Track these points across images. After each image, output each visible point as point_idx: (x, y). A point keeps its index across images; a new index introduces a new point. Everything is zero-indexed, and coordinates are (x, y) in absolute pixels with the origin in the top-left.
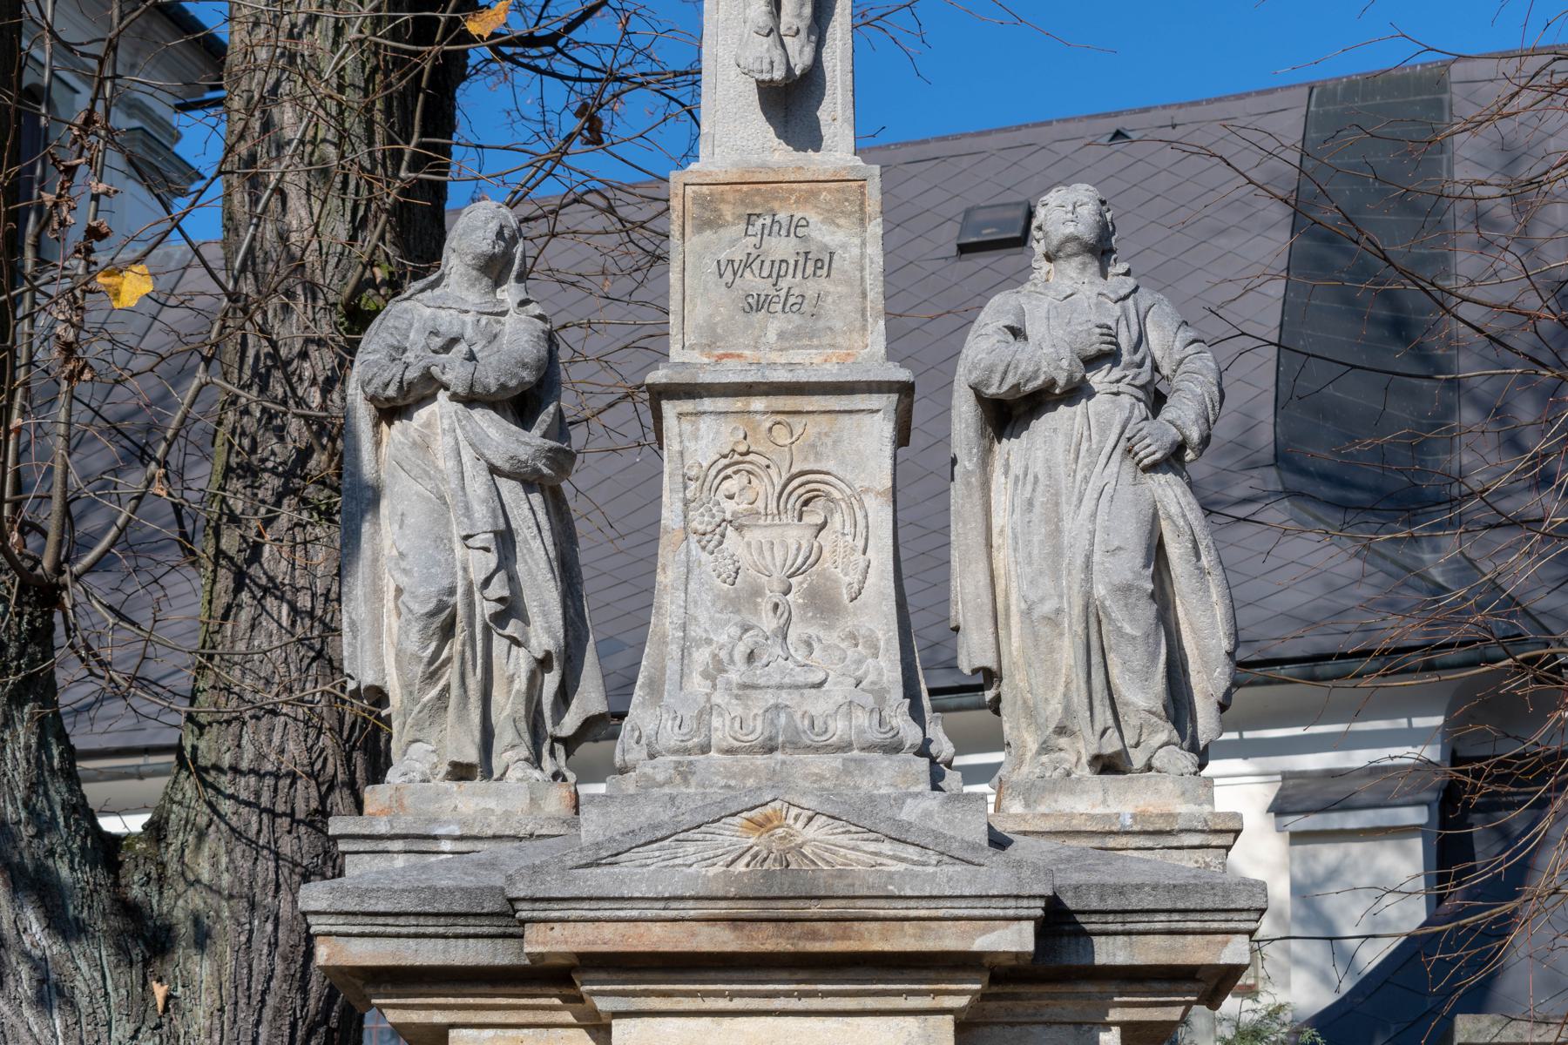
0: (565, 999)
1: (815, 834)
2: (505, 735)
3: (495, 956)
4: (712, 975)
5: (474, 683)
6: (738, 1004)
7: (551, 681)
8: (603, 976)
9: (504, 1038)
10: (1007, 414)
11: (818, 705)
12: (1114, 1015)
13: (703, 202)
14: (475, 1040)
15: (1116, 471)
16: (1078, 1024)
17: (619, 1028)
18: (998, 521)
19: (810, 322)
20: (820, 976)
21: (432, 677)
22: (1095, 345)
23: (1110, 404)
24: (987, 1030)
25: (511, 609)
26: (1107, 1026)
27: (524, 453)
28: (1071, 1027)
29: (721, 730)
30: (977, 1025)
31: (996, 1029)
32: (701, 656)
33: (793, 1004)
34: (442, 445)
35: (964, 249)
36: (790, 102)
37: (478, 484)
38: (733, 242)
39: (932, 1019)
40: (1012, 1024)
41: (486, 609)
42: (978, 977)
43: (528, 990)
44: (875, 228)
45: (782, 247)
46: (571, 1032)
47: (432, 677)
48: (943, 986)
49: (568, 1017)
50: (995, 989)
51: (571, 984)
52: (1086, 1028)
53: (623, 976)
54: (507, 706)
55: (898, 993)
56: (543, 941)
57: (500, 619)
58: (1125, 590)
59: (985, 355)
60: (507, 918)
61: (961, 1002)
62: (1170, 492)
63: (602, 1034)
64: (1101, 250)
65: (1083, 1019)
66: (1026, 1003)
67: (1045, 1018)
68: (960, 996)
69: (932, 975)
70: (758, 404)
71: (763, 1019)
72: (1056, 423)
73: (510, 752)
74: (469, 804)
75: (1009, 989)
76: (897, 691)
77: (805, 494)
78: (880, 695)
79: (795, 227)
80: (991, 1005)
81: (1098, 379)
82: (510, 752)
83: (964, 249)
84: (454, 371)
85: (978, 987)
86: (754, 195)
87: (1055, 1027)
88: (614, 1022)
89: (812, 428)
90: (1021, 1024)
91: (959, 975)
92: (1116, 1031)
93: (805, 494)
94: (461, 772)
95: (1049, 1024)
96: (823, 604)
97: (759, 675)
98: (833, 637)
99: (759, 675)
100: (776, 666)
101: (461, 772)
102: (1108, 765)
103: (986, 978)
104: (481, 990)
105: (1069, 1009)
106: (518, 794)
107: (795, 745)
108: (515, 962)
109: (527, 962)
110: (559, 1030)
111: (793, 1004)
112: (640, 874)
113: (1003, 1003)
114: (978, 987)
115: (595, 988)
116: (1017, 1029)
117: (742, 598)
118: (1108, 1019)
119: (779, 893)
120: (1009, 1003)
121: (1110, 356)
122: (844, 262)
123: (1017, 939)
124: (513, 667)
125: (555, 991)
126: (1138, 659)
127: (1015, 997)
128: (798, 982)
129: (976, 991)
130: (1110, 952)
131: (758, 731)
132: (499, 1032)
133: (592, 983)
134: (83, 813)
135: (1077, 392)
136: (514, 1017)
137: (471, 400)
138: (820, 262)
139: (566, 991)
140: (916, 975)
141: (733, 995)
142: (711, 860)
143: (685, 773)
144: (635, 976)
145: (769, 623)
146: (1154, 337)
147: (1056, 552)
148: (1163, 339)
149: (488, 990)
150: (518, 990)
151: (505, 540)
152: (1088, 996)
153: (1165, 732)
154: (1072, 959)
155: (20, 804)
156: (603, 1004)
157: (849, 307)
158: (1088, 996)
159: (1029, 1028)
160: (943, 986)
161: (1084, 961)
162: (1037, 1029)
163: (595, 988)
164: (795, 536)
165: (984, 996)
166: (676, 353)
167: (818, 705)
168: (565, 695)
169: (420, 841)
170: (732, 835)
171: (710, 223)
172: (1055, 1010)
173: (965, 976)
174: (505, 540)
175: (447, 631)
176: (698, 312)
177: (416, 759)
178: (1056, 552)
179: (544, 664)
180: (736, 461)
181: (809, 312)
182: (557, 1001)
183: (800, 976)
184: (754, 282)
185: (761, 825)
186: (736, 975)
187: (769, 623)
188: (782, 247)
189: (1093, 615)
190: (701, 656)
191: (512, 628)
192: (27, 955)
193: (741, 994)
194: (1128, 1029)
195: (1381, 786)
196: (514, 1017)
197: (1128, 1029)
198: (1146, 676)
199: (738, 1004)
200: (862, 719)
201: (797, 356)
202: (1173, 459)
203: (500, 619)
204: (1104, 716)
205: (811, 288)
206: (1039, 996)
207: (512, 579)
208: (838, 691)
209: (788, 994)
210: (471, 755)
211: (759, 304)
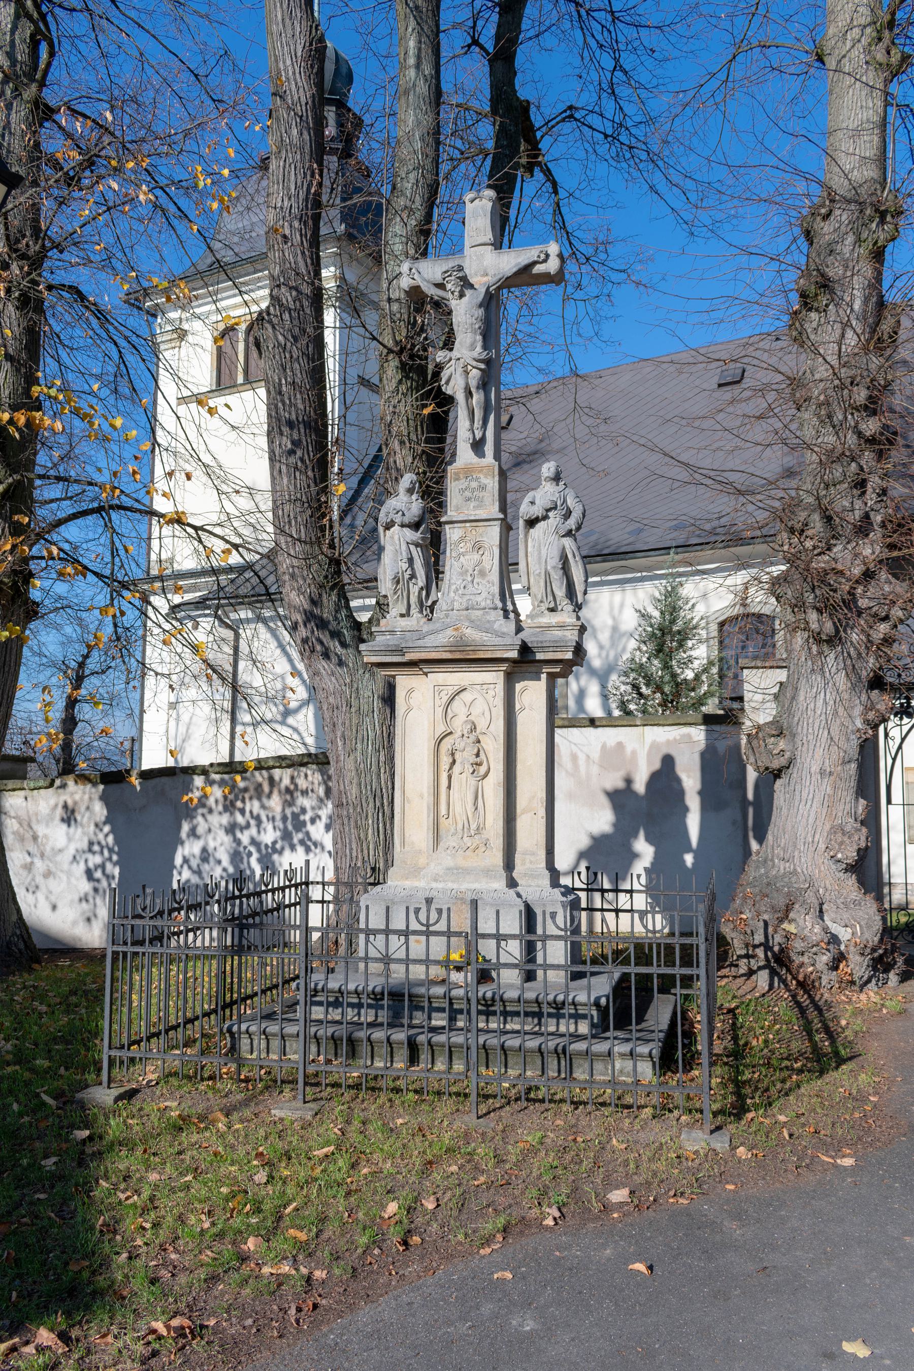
1: (468, 631)
2: (413, 606)
5: (405, 594)
7: (424, 593)
10: (531, 523)
11: (479, 599)
13: (457, 474)
15: (553, 538)
18: (529, 550)
19: (481, 505)
21: (395, 593)
22: (549, 506)
23: (554, 519)
25: (413, 576)
27: (414, 538)
29: (456, 605)
32: (453, 587)
34: (396, 537)
35: (720, 385)
36: (478, 446)
37: (404, 547)
38: (462, 484)
41: (407, 576)
44: (497, 478)
45: (474, 484)
47: (395, 593)
54: (414, 599)
56: (408, 657)
57: (410, 579)
58: (554, 567)
59: (526, 510)
60: (401, 651)
62: (568, 542)
64: (557, 478)
68: (504, 667)
70: (468, 524)
72: (541, 525)
73: (414, 610)
74: (404, 623)
76: (497, 597)
77: (478, 547)
78: (493, 596)
79: (477, 479)
81: (551, 514)
82: (414, 610)
83: (720, 385)
84: (398, 519)
86: (468, 472)
89: (480, 530)
93: (478, 547)
94: (402, 616)
96: (482, 574)
97: (466, 591)
98: (484, 582)
99: (466, 591)
100: (470, 589)
101: (402, 616)
102: (552, 610)
106: (416, 620)
107: (473, 609)
112: (429, 641)
117: (464, 572)
119: (460, 644)
121: (555, 508)
122: (489, 487)
123: (514, 654)
124: (414, 590)
126: (558, 583)
130: (540, 656)
131: (464, 606)
134: (350, 616)
135: (545, 518)
137: (402, 526)
138: (483, 488)
142: (445, 638)
143: (447, 616)
145: (470, 579)
146: (569, 502)
147: (540, 558)
148: (570, 502)
151: (411, 561)
153: (567, 601)
154: (531, 658)
157: (490, 499)
164: (476, 557)
166: (449, 513)
167: (479, 599)
168: (428, 595)
169: (392, 632)
170: (450, 632)
171: (457, 479)
172: (530, 669)
174: (411, 561)
175: (398, 582)
176: (454, 502)
177: (395, 610)
178: (540, 558)
179: (422, 588)
180: (462, 539)
181: (480, 500)
184: (468, 494)
185: (457, 629)
187: (470, 579)
188: (474, 484)
189: (547, 574)
190: (453, 587)
191: (414, 581)
192: (336, 654)
194: (548, 673)
197: (548, 673)
198: (561, 588)
200: (488, 602)
201: (477, 512)
202: (569, 533)
203: (410, 579)
204: (550, 598)
205: (481, 494)
207: (413, 569)
208: (484, 595)
210: (404, 612)
211: (469, 499)
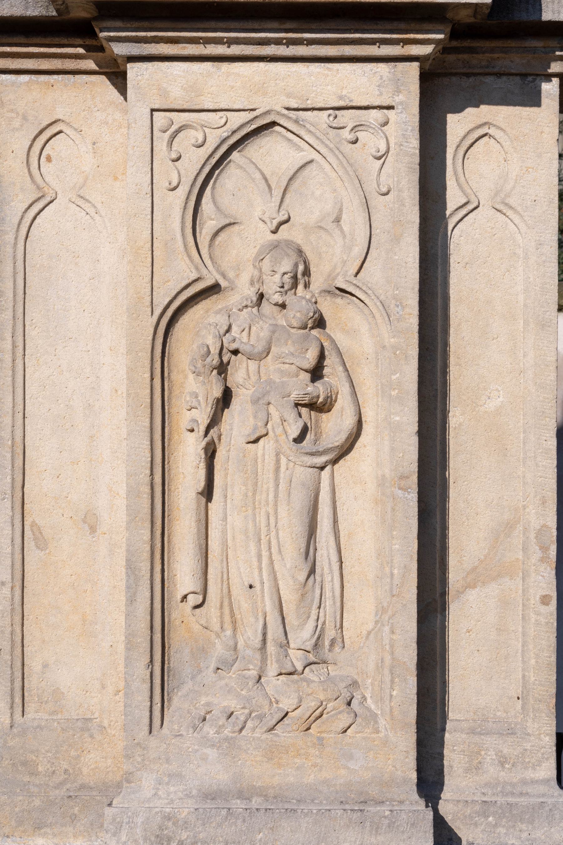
0: (88, 49)
3: (27, 8)
4: (213, 24)
6: (235, 50)
8: (119, 24)
9: (38, 83)
12: (556, 67)
14: (13, 84)
16: (523, 76)
17: (134, 71)
20: (305, 26)
24: (446, 80)
26: (548, 77)
28: (517, 79)
30: (439, 75)
31: (454, 79)
33: (282, 51)
39: (401, 66)
40: (468, 75)
42: (441, 27)
43: (57, 40)
46: (93, 78)
48: (412, 36)
49: (91, 65)
50: (454, 43)
51: (94, 35)
52: (530, 78)
53: (136, 24)
55: (372, 42)
61: (426, 50)
63: (120, 80)
65: (529, 71)
66: (480, 56)
67: (496, 70)
69: (402, 26)
71: (256, 64)
75: (467, 43)
80: (451, 58)
85: (441, 36)
87: (504, 78)
88: (129, 65)
90: (475, 75)
91: (426, 26)
92: (556, 81)
95: (499, 75)
103: (448, 30)
104: (16, 40)
105: (516, 62)
108: (44, 13)
109: (54, 13)
110: (84, 77)
111: (282, 51)
113: (460, 56)
114: (441, 36)
115: (112, 34)
116: (471, 79)
118: (550, 71)
120: (465, 56)
125: (79, 41)
127: (471, 50)
128: (287, 31)
129: (440, 40)
132: (33, 77)
133: (109, 30)
136: (45, 65)
139: (88, 42)
140: (389, 26)
141: (230, 42)
144: (146, 24)
149: (23, 40)
150: (48, 41)
152: (534, 50)
154: (523, 16)
155: (532, 536)
156: (120, 49)
158: (534, 50)
159: (482, 78)
160: (412, 36)
161: (533, 18)
162: (489, 80)
163: (112, 34)
165: (444, 49)
173: (430, 26)
182: (81, 51)
183: (288, 25)
186: (233, 25)
193: (237, 41)
195: (316, 417)
196: (45, 65)
199: (235, 50)
206: (492, 50)
209: (278, 42)
